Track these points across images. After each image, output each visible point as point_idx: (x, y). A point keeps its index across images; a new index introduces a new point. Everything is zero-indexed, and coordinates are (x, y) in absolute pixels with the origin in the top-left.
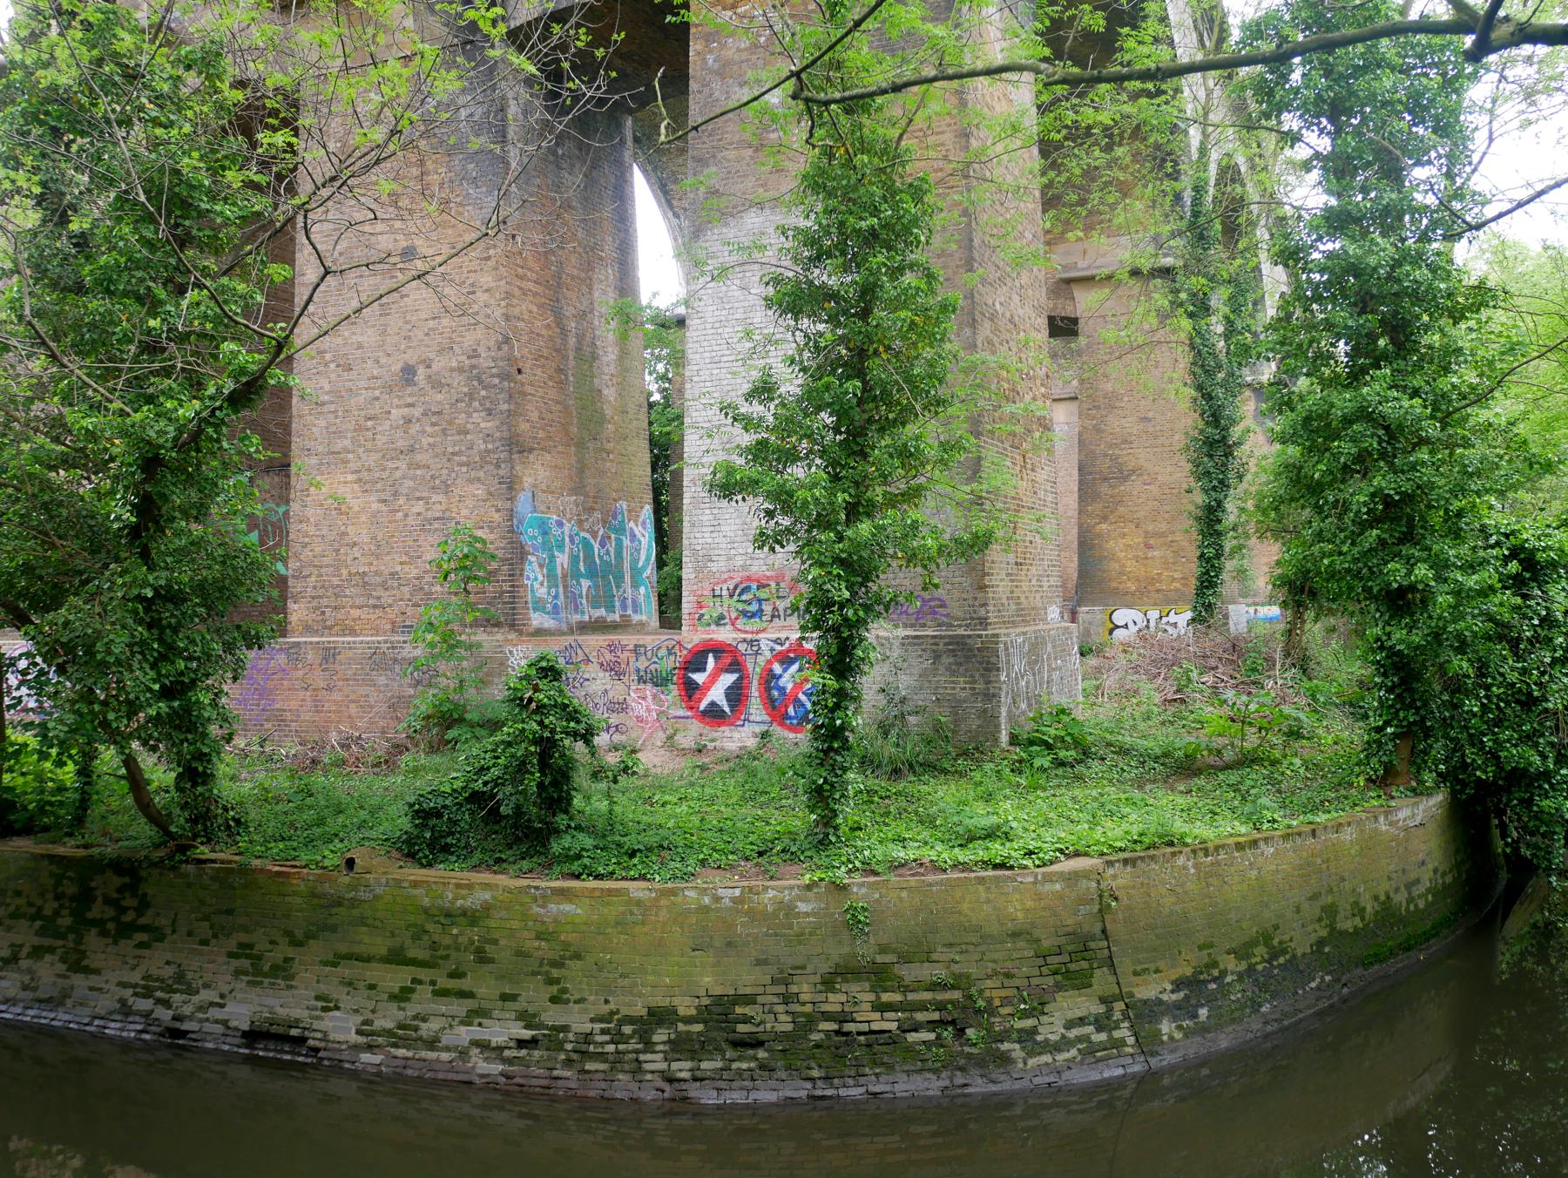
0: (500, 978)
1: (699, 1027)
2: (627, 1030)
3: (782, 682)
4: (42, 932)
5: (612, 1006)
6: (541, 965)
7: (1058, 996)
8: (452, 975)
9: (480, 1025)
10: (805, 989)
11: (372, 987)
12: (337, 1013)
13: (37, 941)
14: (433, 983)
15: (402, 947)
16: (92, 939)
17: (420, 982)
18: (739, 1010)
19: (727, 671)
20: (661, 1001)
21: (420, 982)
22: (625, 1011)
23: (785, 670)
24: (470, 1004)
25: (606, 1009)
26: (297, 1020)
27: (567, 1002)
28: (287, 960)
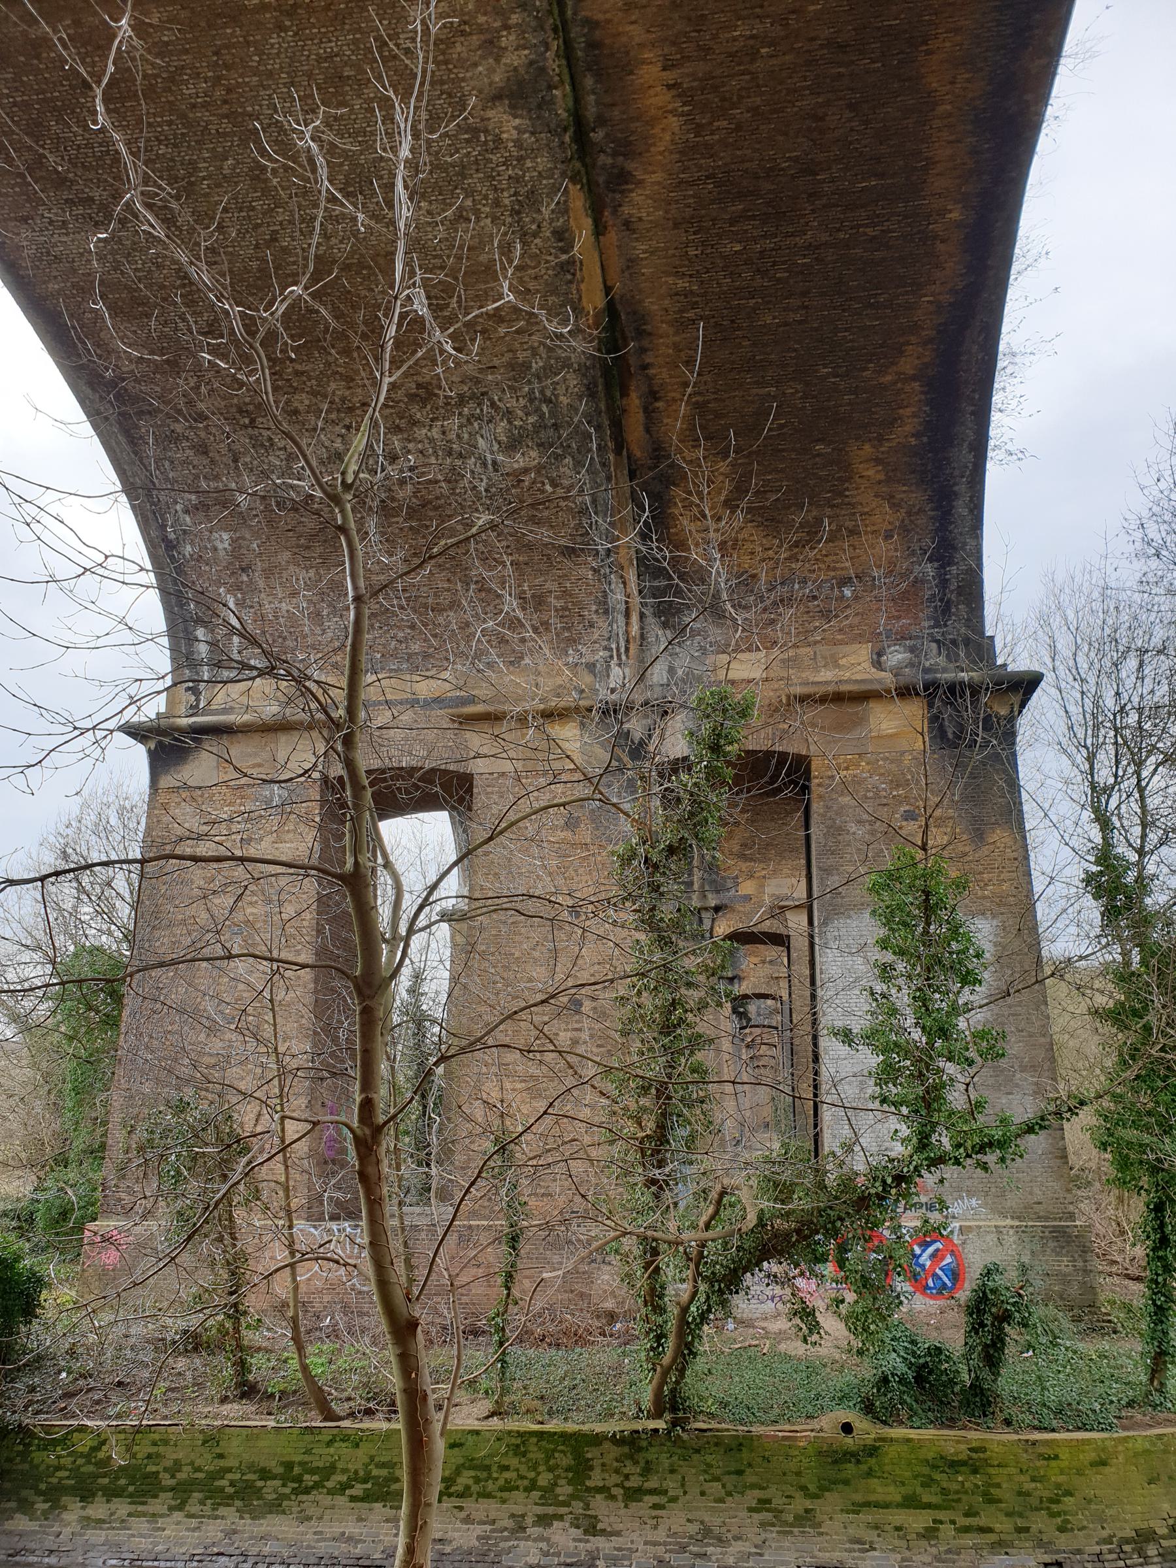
2: (1127, 1548)
3: (921, 1260)
4: (544, 1501)
6: (1041, 1502)
7: (17, 1516)
8: (967, 1515)
9: (1007, 1553)
13: (539, 1510)
14: (953, 1522)
15: (914, 1493)
16: (599, 1504)
17: (941, 1522)
21: (941, 1522)
22: (1120, 1534)
23: (923, 1251)
24: (992, 1537)
25: (1105, 1534)
27: (1072, 1530)
28: (807, 1511)
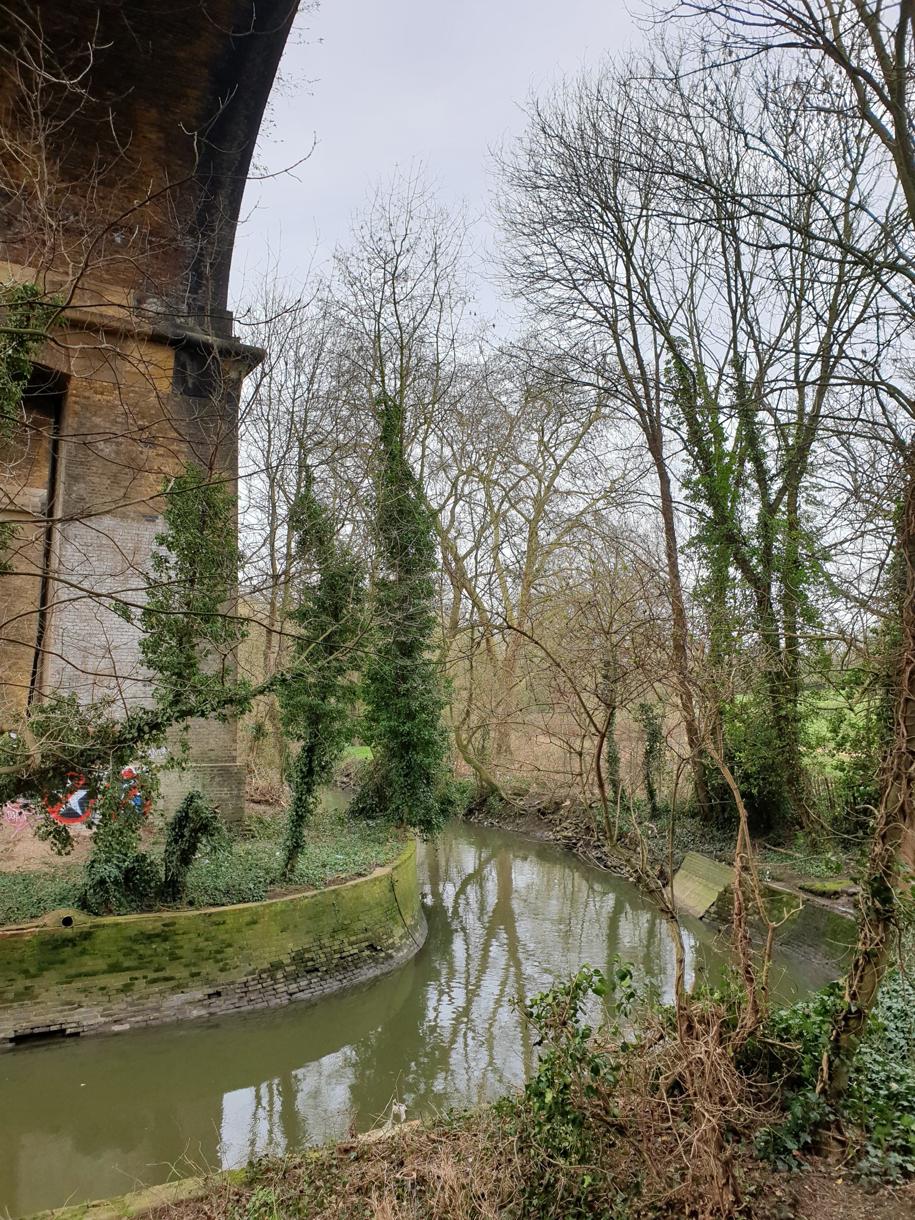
0: (186, 966)
1: (294, 968)
2: (264, 976)
5: (253, 967)
8: (156, 971)
10: (326, 941)
11: (102, 989)
12: (82, 1010)
14: (145, 977)
17: (136, 979)
18: (306, 956)
19: (82, 788)
20: (274, 959)
21: (136, 979)
22: (260, 967)
24: (172, 983)
25: (251, 968)
26: (53, 1021)
28: (27, 988)
